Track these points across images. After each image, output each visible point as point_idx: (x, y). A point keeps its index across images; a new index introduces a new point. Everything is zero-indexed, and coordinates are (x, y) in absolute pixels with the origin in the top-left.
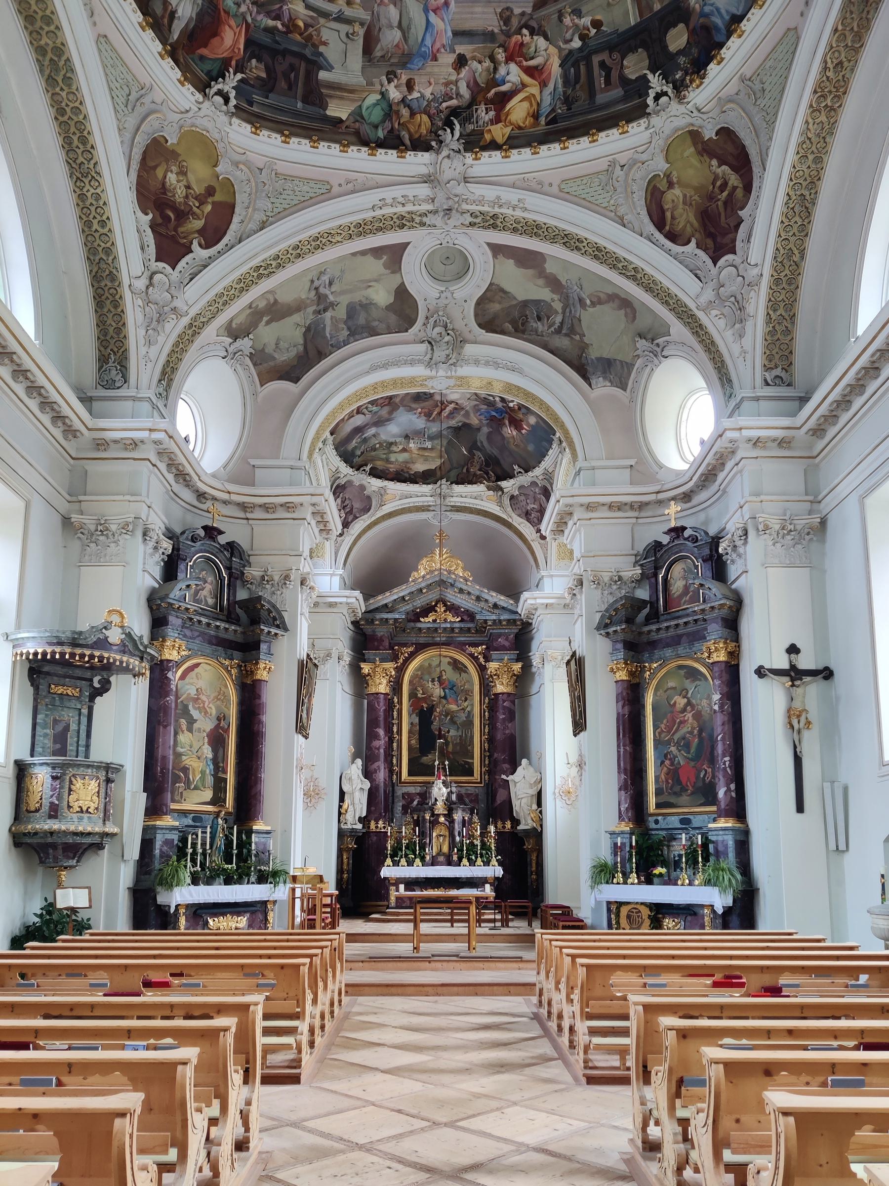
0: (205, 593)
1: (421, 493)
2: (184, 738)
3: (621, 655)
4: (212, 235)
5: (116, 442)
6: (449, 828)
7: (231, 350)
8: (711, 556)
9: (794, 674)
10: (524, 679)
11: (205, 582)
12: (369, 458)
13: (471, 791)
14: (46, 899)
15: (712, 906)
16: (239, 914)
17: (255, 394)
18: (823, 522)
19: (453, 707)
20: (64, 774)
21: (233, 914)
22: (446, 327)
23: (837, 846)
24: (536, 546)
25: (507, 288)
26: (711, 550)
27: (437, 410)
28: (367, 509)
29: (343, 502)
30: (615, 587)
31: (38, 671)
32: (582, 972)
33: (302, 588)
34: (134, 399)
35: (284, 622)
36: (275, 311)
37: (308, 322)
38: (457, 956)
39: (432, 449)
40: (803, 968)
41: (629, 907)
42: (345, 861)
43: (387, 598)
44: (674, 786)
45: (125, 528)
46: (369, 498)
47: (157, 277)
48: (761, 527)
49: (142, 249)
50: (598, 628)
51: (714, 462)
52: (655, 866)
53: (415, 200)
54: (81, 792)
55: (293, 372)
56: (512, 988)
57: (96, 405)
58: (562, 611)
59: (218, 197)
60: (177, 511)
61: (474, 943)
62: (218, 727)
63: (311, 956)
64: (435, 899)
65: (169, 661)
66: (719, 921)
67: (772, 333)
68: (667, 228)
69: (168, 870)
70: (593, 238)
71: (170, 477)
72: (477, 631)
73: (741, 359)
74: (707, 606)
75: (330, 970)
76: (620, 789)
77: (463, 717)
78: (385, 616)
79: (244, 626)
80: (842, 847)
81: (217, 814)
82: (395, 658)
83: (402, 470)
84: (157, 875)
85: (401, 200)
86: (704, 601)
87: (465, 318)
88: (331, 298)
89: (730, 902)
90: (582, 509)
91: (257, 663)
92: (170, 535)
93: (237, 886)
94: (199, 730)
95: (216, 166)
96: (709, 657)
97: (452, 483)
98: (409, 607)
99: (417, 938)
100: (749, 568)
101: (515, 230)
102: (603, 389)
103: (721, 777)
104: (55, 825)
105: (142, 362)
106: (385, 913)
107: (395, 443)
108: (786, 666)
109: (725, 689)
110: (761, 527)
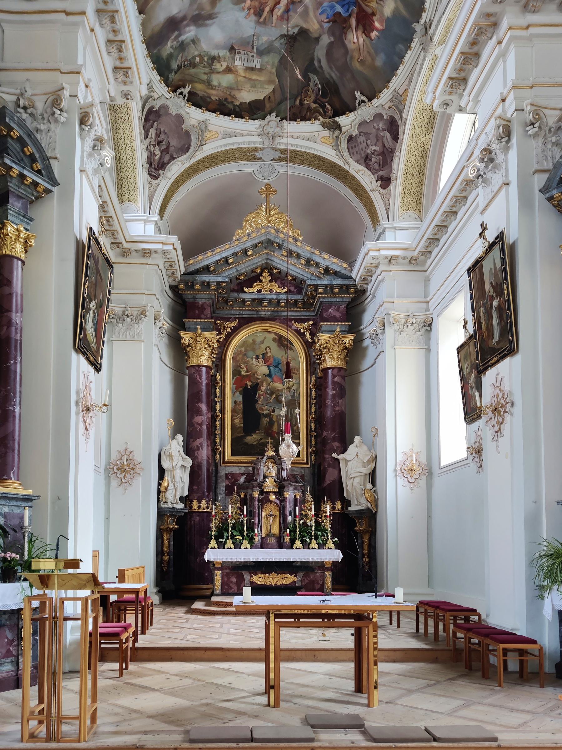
6: (280, 507)
12: (188, 78)
19: (278, 386)
24: (376, 198)
28: (185, 149)
29: (158, 135)
33: (82, 130)
39: (260, 70)
42: (166, 542)
43: (209, 258)
46: (187, 134)
78: (207, 278)
83: (226, 99)
97: (282, 120)
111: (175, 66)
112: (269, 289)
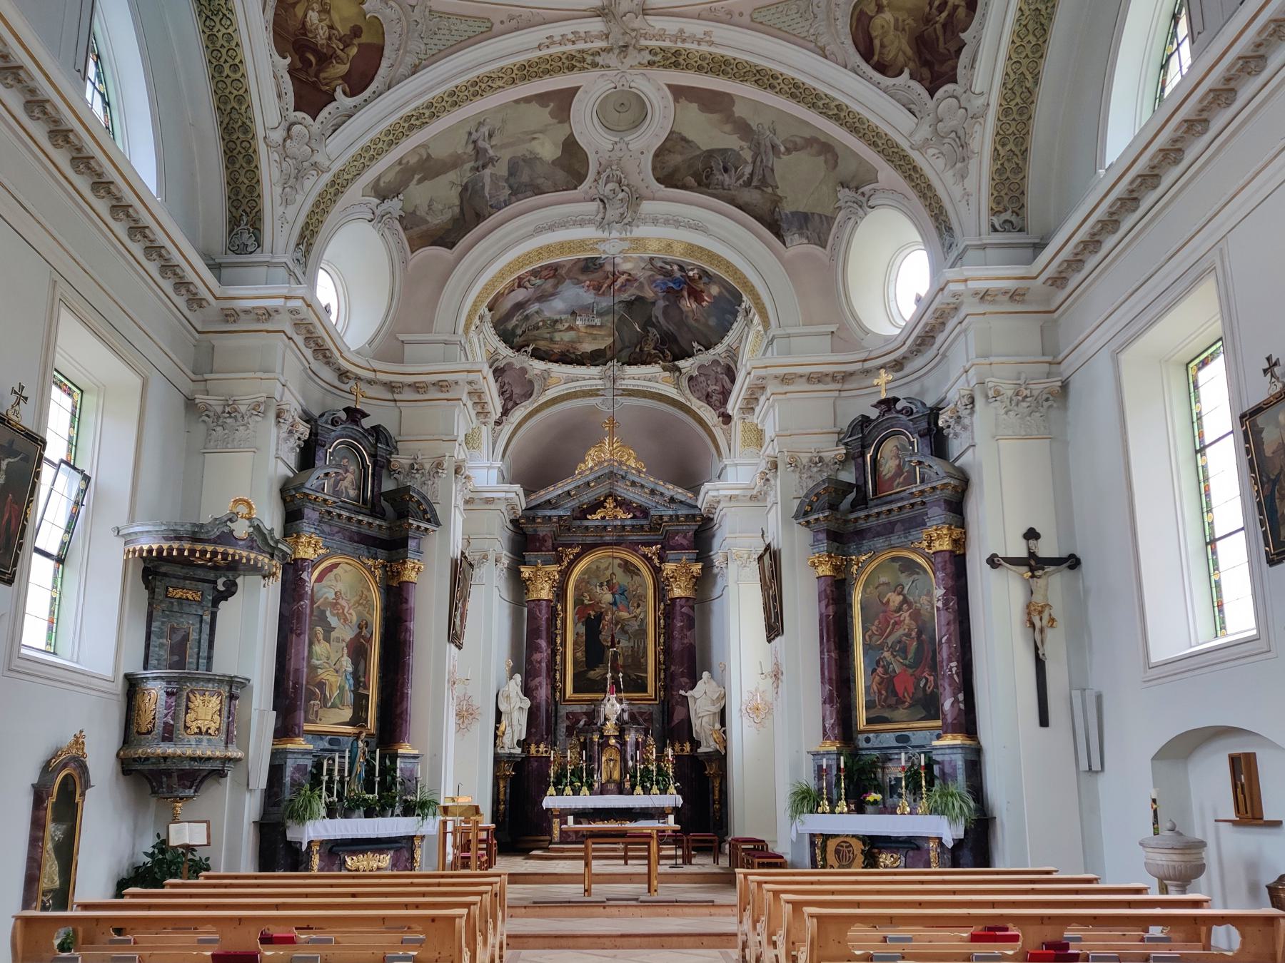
0: (346, 483)
1: (589, 375)
2: (320, 648)
3: (824, 547)
4: (358, 82)
5: (246, 312)
7: (377, 212)
8: (929, 430)
9: (1034, 563)
10: (704, 582)
11: (347, 471)
13: (645, 709)
14: (158, 836)
15: (940, 839)
16: (381, 852)
17: (405, 262)
18: (1065, 386)
19: (624, 615)
20: (180, 690)
21: (374, 851)
22: (620, 182)
23: (1090, 766)
24: (718, 432)
25: (690, 136)
26: (929, 424)
27: (608, 282)
28: (528, 395)
30: (815, 470)
31: (155, 572)
32: (811, 925)
34: (269, 264)
35: (435, 516)
36: (427, 168)
37: (465, 180)
38: (636, 900)
40: (1095, 917)
41: (838, 840)
42: (502, 790)
43: (551, 493)
44: (888, 696)
45: (256, 409)
46: (531, 382)
47: (296, 128)
48: (991, 393)
49: (279, 97)
50: (796, 517)
51: (933, 321)
52: (867, 792)
53: (587, 37)
54: (200, 710)
55: (447, 237)
56: (705, 939)
57: (225, 272)
58: (751, 498)
59: (365, 39)
60: (316, 393)
61: (655, 882)
62: (359, 635)
63: (468, 905)
64: (607, 832)
65: (304, 560)
66: (947, 856)
67: (1001, 171)
68: (876, 58)
69: (299, 801)
70: (790, 73)
71: (309, 353)
72: (651, 529)
73: (964, 202)
74: (927, 487)
75: (490, 920)
76: (824, 702)
77: (635, 625)
79: (390, 520)
80: (1096, 767)
81: (357, 736)
82: (559, 561)
84: (287, 807)
85: (571, 36)
86: (922, 481)
87: (643, 174)
88: (491, 152)
89: (961, 834)
90: (776, 382)
91: (405, 562)
92: (308, 418)
93: (380, 819)
94: (338, 640)
95: (362, 3)
96: (929, 547)
98: (574, 503)
99: (587, 879)
100: (976, 440)
101: (700, 69)
102: (798, 247)
103: (946, 686)
104: (170, 749)
105: (278, 224)
106: (547, 849)
107: (561, 321)
108: (1024, 554)
109: (950, 583)
110: (991, 393)
111: (519, 332)
112: (612, 515)
